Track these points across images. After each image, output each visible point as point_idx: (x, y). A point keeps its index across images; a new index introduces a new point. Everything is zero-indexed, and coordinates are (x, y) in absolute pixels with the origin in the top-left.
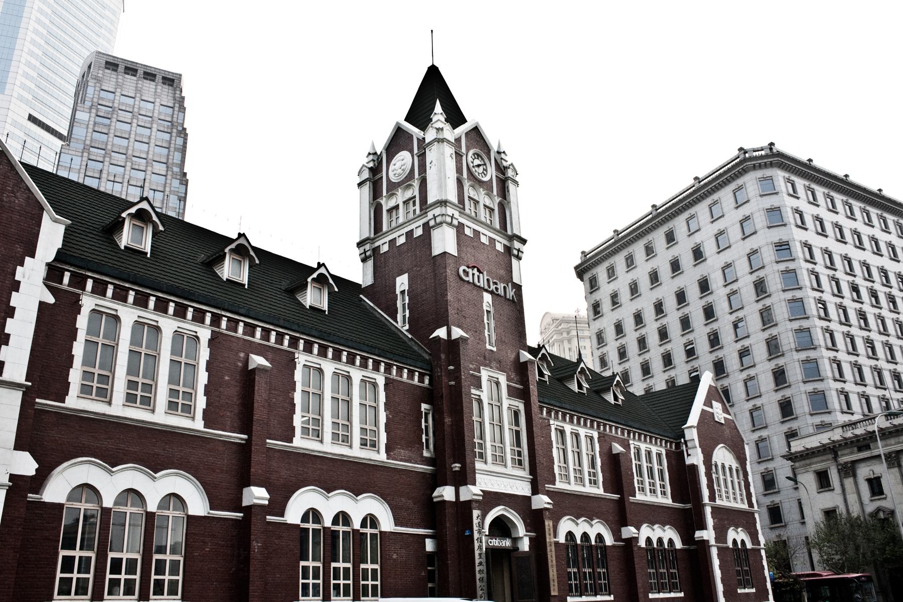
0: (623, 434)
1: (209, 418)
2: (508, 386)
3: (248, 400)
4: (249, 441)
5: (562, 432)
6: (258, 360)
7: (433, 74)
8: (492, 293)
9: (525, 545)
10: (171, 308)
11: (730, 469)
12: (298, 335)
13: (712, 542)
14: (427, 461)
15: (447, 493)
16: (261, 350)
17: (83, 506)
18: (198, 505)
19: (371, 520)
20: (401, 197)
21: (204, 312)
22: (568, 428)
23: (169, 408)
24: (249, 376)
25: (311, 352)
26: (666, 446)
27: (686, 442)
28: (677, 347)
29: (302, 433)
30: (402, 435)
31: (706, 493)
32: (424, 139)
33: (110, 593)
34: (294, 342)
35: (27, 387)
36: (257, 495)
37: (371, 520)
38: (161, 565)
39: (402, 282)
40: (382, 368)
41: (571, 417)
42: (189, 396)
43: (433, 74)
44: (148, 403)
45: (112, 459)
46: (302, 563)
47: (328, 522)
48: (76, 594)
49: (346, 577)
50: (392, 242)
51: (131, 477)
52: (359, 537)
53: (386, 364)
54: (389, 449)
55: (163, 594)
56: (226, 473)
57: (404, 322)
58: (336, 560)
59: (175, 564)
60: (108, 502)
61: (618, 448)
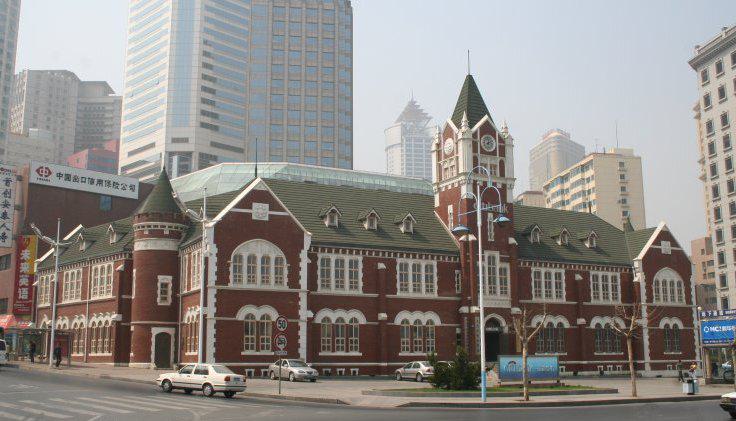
0: (389, 255)
1: (365, 290)
3: (380, 281)
4: (379, 297)
6: (381, 266)
9: (506, 330)
11: (672, 283)
14: (458, 295)
15: (464, 309)
16: (577, 272)
17: (250, 321)
18: (362, 320)
24: (576, 283)
30: (446, 283)
31: (644, 298)
34: (395, 255)
36: (383, 316)
38: (263, 340)
39: (450, 209)
42: (356, 283)
44: (419, 290)
45: (334, 308)
47: (424, 324)
50: (446, 187)
51: (340, 313)
56: (368, 307)
60: (333, 322)
61: (578, 277)
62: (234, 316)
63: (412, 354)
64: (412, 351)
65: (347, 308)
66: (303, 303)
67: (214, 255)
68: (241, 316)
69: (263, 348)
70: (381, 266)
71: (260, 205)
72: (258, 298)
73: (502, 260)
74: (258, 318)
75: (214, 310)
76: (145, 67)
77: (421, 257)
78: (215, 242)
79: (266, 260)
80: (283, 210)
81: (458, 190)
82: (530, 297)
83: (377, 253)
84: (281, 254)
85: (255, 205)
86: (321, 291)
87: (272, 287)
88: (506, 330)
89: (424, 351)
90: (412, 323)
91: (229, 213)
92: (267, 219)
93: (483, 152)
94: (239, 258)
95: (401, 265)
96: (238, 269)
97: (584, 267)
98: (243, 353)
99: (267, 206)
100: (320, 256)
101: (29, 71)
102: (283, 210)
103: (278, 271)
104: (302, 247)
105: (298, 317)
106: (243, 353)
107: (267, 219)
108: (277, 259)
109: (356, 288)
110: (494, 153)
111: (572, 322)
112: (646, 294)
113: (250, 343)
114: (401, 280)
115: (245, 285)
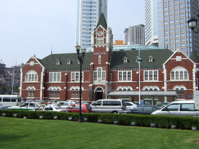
1: (133, 80)
38: (181, 96)
62: (26, 89)
68: (27, 89)
69: (76, 97)
71: (179, 57)
72: (31, 84)
73: (103, 69)
74: (75, 90)
75: (21, 88)
79: (33, 75)
80: (37, 62)
82: (117, 81)
83: (65, 71)
84: (37, 73)
85: (177, 57)
87: (184, 80)
88: (104, 91)
89: (75, 98)
90: (180, 89)
91: (170, 60)
92: (181, 61)
93: (98, 37)
94: (173, 73)
99: (181, 57)
101: (130, 27)
102: (37, 62)
104: (42, 71)
105: (40, 89)
107: (181, 61)
108: (185, 72)
109: (59, 81)
110: (102, 36)
111: (62, 88)
113: (182, 97)
115: (175, 80)
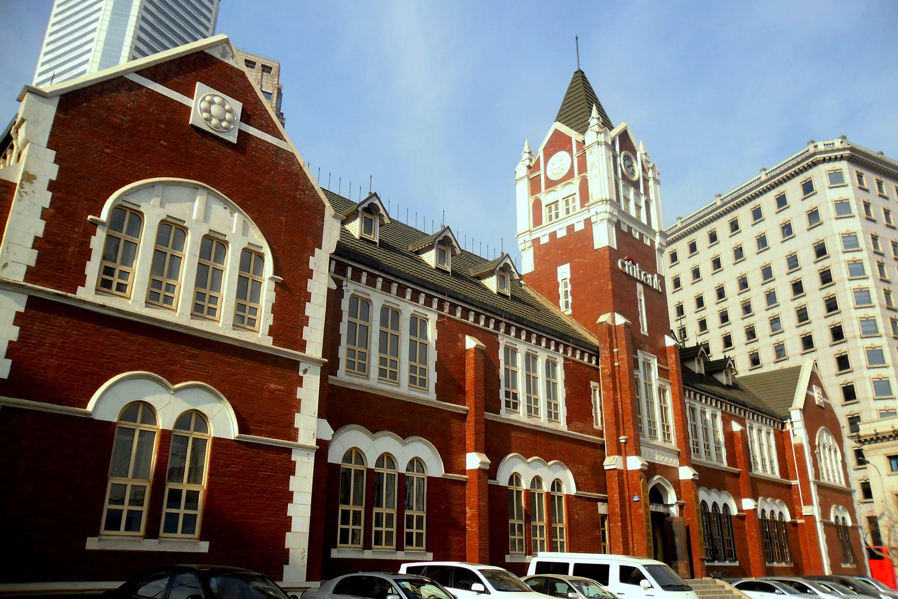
2: (659, 368)
5: (693, 410)
7: (580, 79)
8: (642, 283)
10: (379, 282)
12: (481, 311)
13: (818, 518)
19: (416, 463)
20: (560, 192)
21: (432, 297)
22: (698, 406)
23: (380, 375)
25: (359, 280)
26: (565, 352)
27: (792, 423)
28: (761, 320)
29: (348, 367)
32: (584, 141)
33: (166, 530)
35: (324, 364)
37: (416, 463)
38: (175, 496)
40: (561, 350)
41: (529, 334)
43: (580, 79)
45: (374, 427)
46: (342, 507)
47: (371, 463)
48: (127, 529)
49: (389, 524)
51: (387, 443)
52: (374, 479)
53: (369, 274)
54: (569, 421)
55: (118, 529)
57: (567, 306)
58: (379, 505)
59: (420, 519)
63: (368, 555)
64: (152, 533)
65: (404, 432)
66: (309, 392)
67: (42, 184)
68: (104, 403)
69: (171, 527)
70: (471, 343)
76: (581, 121)
77: (371, 283)
78: (52, 144)
81: (587, 234)
84: (257, 238)
86: (343, 376)
90: (165, 421)
94: (128, 218)
95: (354, 298)
96: (120, 251)
97: (453, 307)
98: (92, 544)
100: (350, 288)
103: (247, 288)
105: (291, 433)
106: (92, 544)
112: (276, 309)
114: (351, 340)
